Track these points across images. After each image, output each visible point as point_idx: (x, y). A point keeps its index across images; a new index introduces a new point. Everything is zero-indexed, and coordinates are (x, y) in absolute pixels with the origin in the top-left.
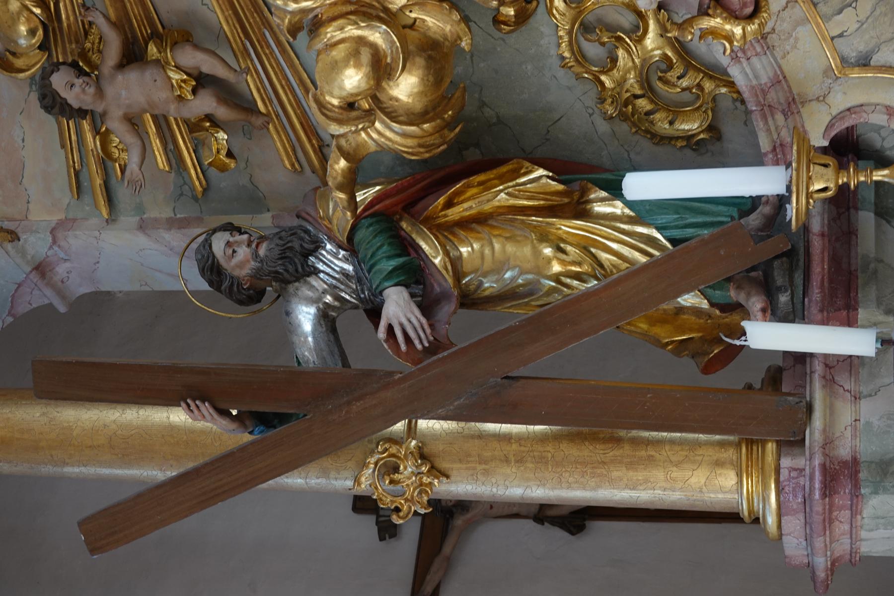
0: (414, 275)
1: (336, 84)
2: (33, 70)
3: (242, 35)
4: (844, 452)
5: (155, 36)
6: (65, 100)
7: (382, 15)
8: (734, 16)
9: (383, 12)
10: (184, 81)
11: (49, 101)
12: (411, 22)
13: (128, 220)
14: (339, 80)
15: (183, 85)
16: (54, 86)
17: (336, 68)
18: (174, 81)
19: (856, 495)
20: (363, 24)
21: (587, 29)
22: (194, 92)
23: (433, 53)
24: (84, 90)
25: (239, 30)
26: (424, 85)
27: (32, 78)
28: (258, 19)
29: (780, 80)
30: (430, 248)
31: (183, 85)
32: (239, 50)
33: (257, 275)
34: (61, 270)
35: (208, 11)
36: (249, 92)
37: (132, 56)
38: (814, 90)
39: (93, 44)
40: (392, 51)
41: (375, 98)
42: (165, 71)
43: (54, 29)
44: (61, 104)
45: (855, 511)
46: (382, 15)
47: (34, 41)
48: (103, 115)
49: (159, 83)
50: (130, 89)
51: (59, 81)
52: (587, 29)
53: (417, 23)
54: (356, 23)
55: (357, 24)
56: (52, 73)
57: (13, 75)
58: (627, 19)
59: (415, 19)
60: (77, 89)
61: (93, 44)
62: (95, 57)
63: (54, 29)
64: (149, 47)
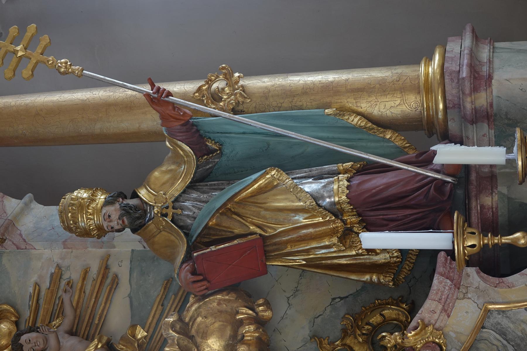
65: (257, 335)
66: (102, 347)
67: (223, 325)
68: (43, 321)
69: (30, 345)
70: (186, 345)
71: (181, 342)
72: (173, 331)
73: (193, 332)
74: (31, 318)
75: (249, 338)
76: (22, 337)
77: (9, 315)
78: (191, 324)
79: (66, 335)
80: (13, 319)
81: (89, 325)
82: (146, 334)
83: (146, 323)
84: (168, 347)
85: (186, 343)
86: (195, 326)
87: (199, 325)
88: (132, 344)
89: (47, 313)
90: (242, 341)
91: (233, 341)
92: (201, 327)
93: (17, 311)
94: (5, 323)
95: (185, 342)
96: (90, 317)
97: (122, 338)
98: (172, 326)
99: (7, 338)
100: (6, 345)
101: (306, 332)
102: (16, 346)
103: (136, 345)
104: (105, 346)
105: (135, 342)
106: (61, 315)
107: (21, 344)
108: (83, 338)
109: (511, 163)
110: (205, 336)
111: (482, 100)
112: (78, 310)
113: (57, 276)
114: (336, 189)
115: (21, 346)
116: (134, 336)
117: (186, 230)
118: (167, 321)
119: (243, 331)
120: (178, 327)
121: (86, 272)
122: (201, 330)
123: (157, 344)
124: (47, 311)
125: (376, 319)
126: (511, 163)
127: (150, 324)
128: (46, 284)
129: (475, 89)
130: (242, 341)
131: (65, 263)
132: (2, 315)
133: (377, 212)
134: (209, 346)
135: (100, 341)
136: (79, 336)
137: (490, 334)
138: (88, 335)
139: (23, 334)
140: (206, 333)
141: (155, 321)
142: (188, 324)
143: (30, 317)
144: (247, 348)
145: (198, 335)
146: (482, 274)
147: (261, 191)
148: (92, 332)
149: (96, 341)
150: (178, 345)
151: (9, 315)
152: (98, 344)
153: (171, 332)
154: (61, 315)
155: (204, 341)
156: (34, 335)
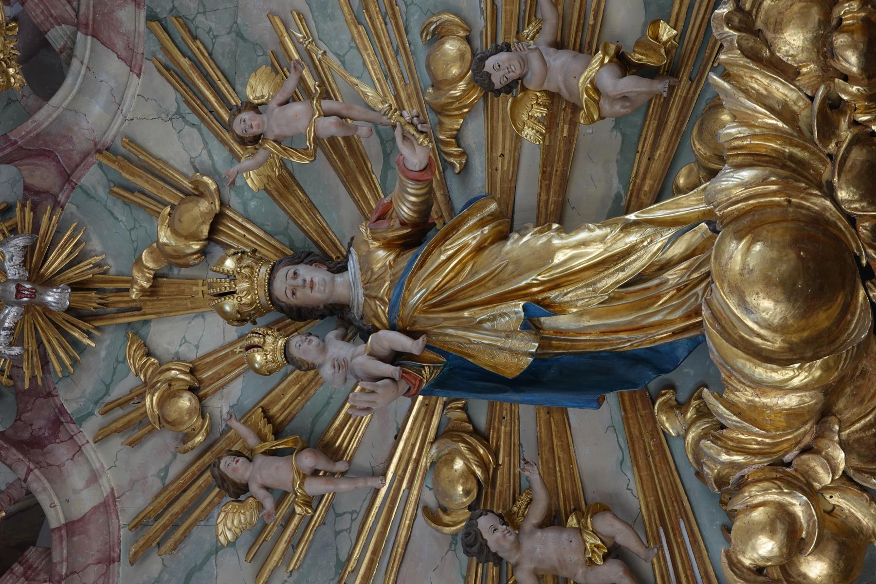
1: (750, 543)
2: (458, 527)
3: (658, 522)
5: (577, 509)
6: (486, 541)
7: (805, 487)
9: (805, 485)
10: (597, 546)
11: (471, 538)
12: (830, 508)
14: (753, 541)
15: (596, 549)
16: (479, 527)
17: (751, 532)
18: (588, 545)
20: (786, 491)
22: (605, 558)
24: (504, 536)
25: (657, 516)
26: (834, 568)
27: (454, 535)
28: (677, 508)
31: (596, 549)
32: (652, 535)
35: (630, 496)
36: (652, 579)
37: (553, 520)
39: (520, 508)
40: (808, 526)
41: (783, 568)
42: (582, 535)
43: (486, 493)
44: (481, 544)
46: (805, 487)
47: (465, 500)
48: (515, 566)
49: (574, 544)
50: (547, 547)
51: (484, 523)
53: (835, 511)
54: (780, 488)
55: (781, 489)
56: (481, 516)
57: (440, 527)
59: (834, 506)
60: (498, 534)
61: (520, 508)
62: (520, 519)
63: (486, 493)
64: (570, 519)
65: (863, 14)
66: (610, 61)
67: (803, 7)
68: (507, 31)
69: (501, 73)
70: (751, 47)
71: (744, 42)
72: (730, 28)
73: (759, 24)
74: (489, 29)
75: (851, 21)
76: (487, 62)
77: (454, 28)
78: (754, 12)
79: (552, 50)
80: (462, 33)
81: (581, 28)
82: (675, 32)
83: (670, 16)
84: (725, 54)
85: (751, 44)
86: (762, 15)
87: (767, 12)
88: (655, 51)
89: (511, 18)
90: (839, 27)
91: (825, 29)
92: (771, 14)
93: (464, 20)
94: (451, 42)
95: (751, 42)
96: (579, 16)
97: (638, 43)
98: (728, 20)
99: (458, 64)
100: (459, 74)
102: (481, 77)
103: (663, 51)
104: (615, 60)
105: (660, 47)
106: (533, 18)
107: (487, 73)
108: (574, 49)
110: (779, 27)
112: (560, 8)
115: (489, 75)
116: (657, 38)
118: (718, 14)
119: (840, 12)
120: (736, 20)
122: (772, 20)
123: (694, 44)
124: (511, 15)
127: (678, 15)
130: (839, 27)
132: (444, 30)
134: (787, 43)
135: (605, 53)
136: (568, 48)
138: (581, 45)
139: (487, 57)
140: (781, 24)
141: (684, 9)
142: (749, 13)
143: (486, 26)
144: (850, 39)
145: (767, 28)
146: (429, 521)
148: (587, 38)
149: (600, 55)
150: (740, 48)
151: (454, 28)
152: (604, 58)
153: (727, 29)
154: (533, 18)
155: (778, 36)
156: (503, 56)
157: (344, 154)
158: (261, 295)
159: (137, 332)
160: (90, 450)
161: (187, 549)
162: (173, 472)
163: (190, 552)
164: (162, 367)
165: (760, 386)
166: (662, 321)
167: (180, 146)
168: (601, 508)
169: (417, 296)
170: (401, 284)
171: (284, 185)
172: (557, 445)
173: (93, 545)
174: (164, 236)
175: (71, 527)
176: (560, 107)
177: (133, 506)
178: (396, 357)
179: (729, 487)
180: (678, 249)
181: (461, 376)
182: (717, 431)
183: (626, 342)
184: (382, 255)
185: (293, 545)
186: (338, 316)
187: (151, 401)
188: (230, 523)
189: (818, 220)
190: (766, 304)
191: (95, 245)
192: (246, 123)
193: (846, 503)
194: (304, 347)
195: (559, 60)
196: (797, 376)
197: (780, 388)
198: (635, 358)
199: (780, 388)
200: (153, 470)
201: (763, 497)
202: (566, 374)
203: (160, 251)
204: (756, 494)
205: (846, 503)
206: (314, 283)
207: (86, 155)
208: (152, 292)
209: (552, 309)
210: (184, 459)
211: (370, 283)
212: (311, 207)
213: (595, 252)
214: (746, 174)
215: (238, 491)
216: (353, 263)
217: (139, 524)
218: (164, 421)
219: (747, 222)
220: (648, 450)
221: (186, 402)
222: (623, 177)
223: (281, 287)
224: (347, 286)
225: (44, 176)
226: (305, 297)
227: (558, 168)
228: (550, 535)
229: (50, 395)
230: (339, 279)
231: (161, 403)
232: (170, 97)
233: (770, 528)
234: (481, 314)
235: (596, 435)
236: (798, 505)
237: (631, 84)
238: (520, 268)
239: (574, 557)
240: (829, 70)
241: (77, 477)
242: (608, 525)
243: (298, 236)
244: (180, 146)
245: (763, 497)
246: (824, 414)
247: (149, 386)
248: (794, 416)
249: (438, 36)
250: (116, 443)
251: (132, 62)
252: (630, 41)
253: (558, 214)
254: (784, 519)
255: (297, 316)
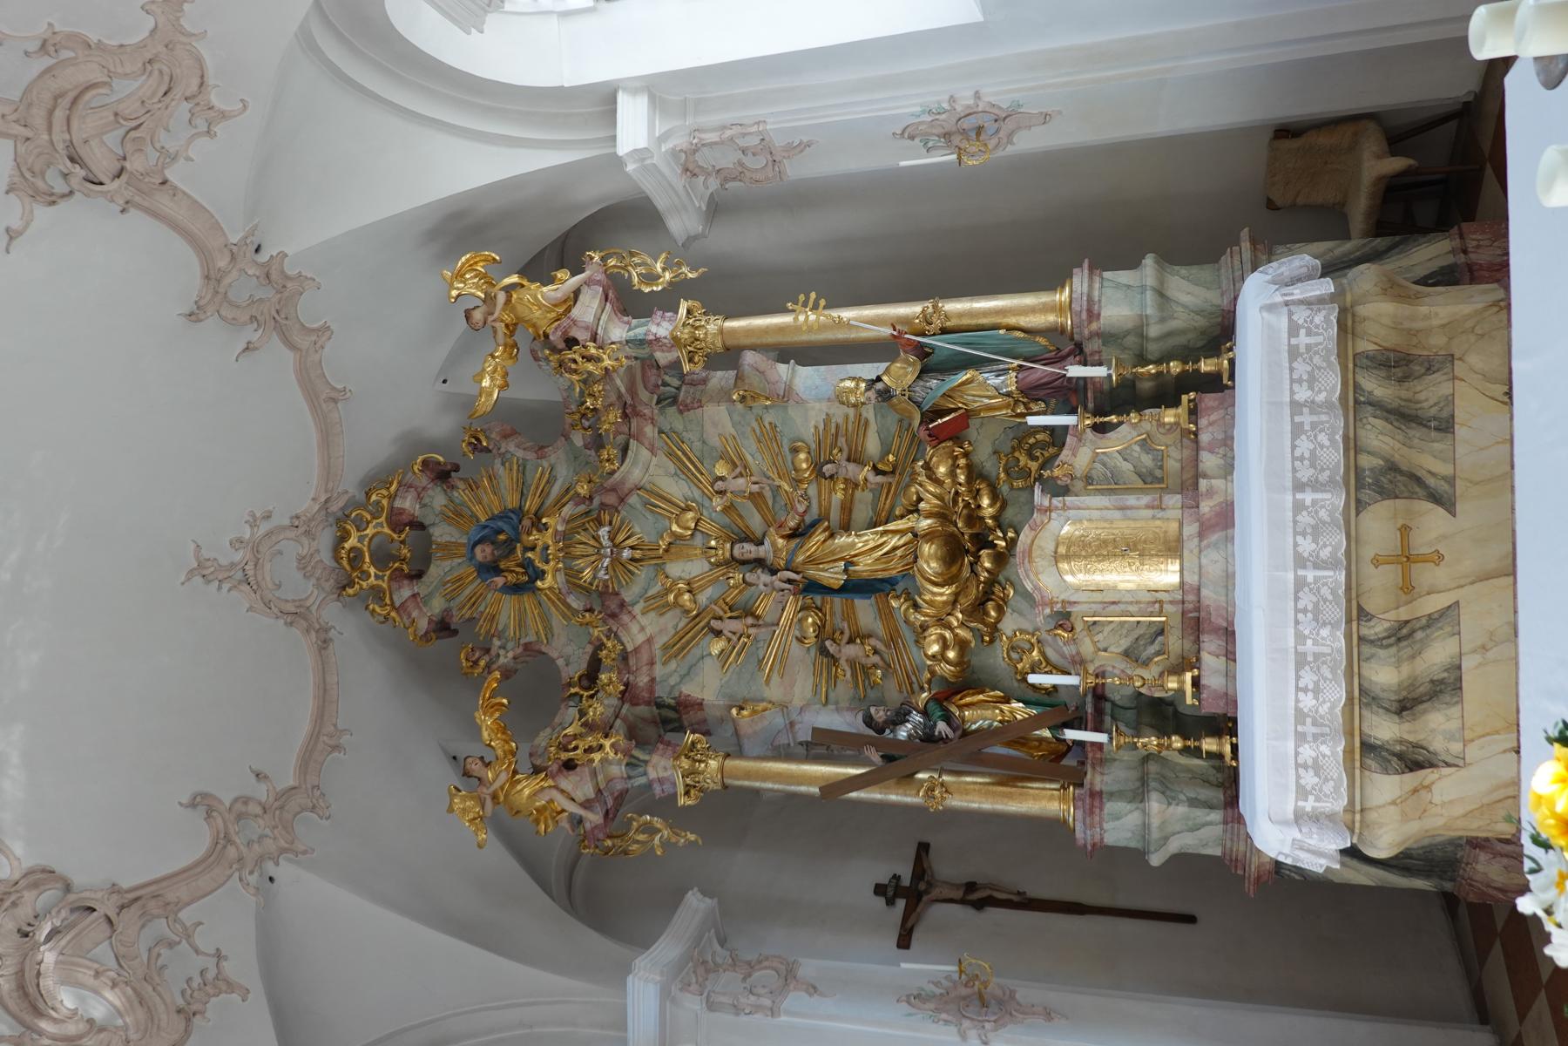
0: (948, 718)
4: (1097, 788)
8: (1065, 630)
13: (831, 707)
19: (1102, 803)
21: (1013, 648)
23: (962, 645)
29: (1078, 653)
30: (953, 709)
33: (885, 722)
34: (797, 727)
37: (851, 641)
38: (1089, 658)
45: (1101, 809)
52: (1013, 648)
58: (1027, 646)
101: (990, 450)
109: (1110, 376)
111: (1094, 326)
113: (827, 422)
114: (1010, 382)
117: (918, 405)
121: (847, 417)
125: (1032, 441)
126: (1110, 376)
128: (821, 427)
129: (1090, 322)
131: (831, 412)
133: (1032, 394)
137: (1098, 466)
147: (963, 383)
157: (757, 498)
158: (728, 555)
159: (660, 568)
160: (639, 617)
161: (689, 657)
162: (681, 625)
163: (690, 659)
164: (674, 583)
165: (934, 594)
166: (894, 569)
167: (677, 489)
168: (870, 636)
169: (800, 558)
170: (794, 553)
171: (729, 509)
172: (850, 615)
173: (645, 657)
174: (675, 528)
175: (637, 650)
176: (851, 485)
177: (659, 642)
178: (789, 581)
179: (924, 628)
180: (902, 542)
181: (813, 587)
182: (916, 606)
183: (880, 575)
184: (780, 541)
185: (739, 654)
186: (759, 563)
187: (671, 597)
188: (717, 646)
189: (952, 535)
190: (934, 565)
191: (637, 529)
192: (720, 485)
193: (961, 632)
194: (750, 577)
195: (852, 467)
196: (947, 590)
197: (942, 594)
198: (882, 580)
199: (942, 594)
200: (670, 625)
201: (934, 632)
202: (857, 587)
203: (673, 533)
204: (932, 630)
205: (961, 632)
206: (747, 550)
207: (631, 491)
208: (666, 551)
209: (853, 564)
210: (684, 621)
211: (776, 550)
212: (741, 517)
213: (872, 544)
214: (929, 521)
215: (718, 633)
216: (767, 542)
217: (666, 648)
218: (676, 604)
219: (929, 536)
220: (886, 614)
221: (687, 596)
222: (874, 510)
223: (736, 552)
224: (764, 551)
225: (611, 499)
226: (747, 556)
227: (847, 508)
228: (851, 646)
229: (617, 594)
230: (761, 548)
231: (676, 597)
232: (672, 468)
233: (937, 641)
234: (826, 566)
235: (865, 611)
236: (948, 634)
237: (880, 479)
238: (842, 548)
239: (861, 654)
240: (955, 482)
241: (635, 628)
242: (873, 641)
243: (736, 529)
244: (677, 489)
245: (934, 632)
246: (955, 602)
247: (668, 591)
248: (944, 603)
249: (795, 451)
250: (652, 614)
251: (652, 451)
252: (876, 459)
253: (846, 527)
254: (943, 638)
255: (735, 562)
